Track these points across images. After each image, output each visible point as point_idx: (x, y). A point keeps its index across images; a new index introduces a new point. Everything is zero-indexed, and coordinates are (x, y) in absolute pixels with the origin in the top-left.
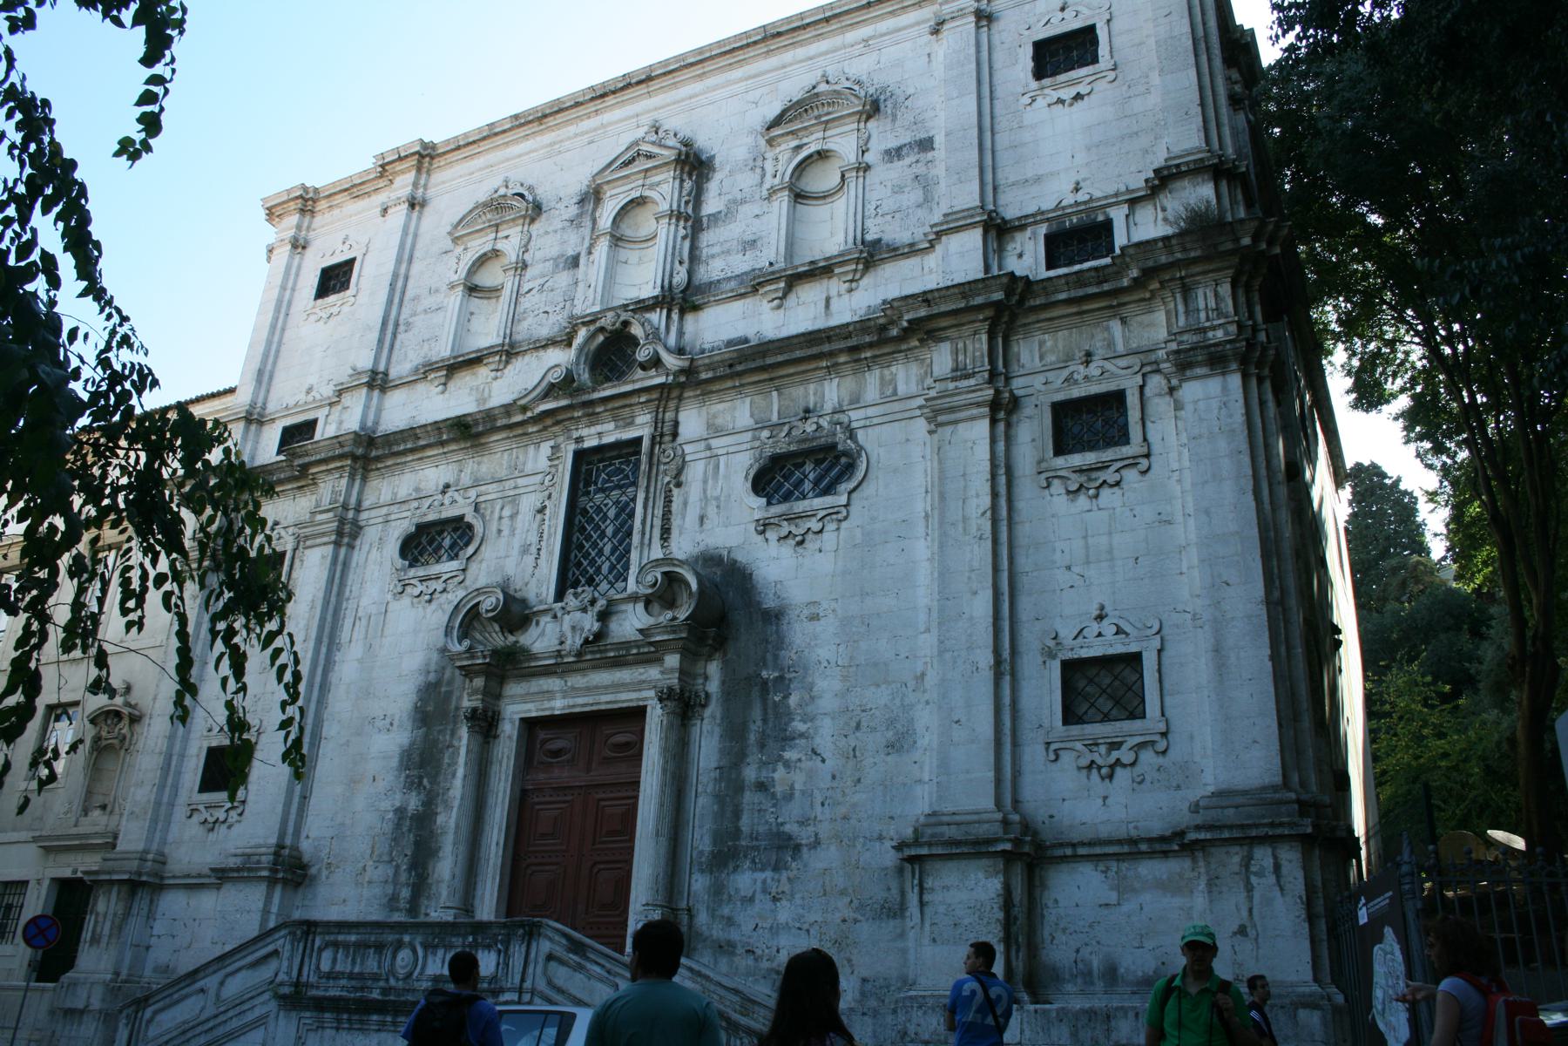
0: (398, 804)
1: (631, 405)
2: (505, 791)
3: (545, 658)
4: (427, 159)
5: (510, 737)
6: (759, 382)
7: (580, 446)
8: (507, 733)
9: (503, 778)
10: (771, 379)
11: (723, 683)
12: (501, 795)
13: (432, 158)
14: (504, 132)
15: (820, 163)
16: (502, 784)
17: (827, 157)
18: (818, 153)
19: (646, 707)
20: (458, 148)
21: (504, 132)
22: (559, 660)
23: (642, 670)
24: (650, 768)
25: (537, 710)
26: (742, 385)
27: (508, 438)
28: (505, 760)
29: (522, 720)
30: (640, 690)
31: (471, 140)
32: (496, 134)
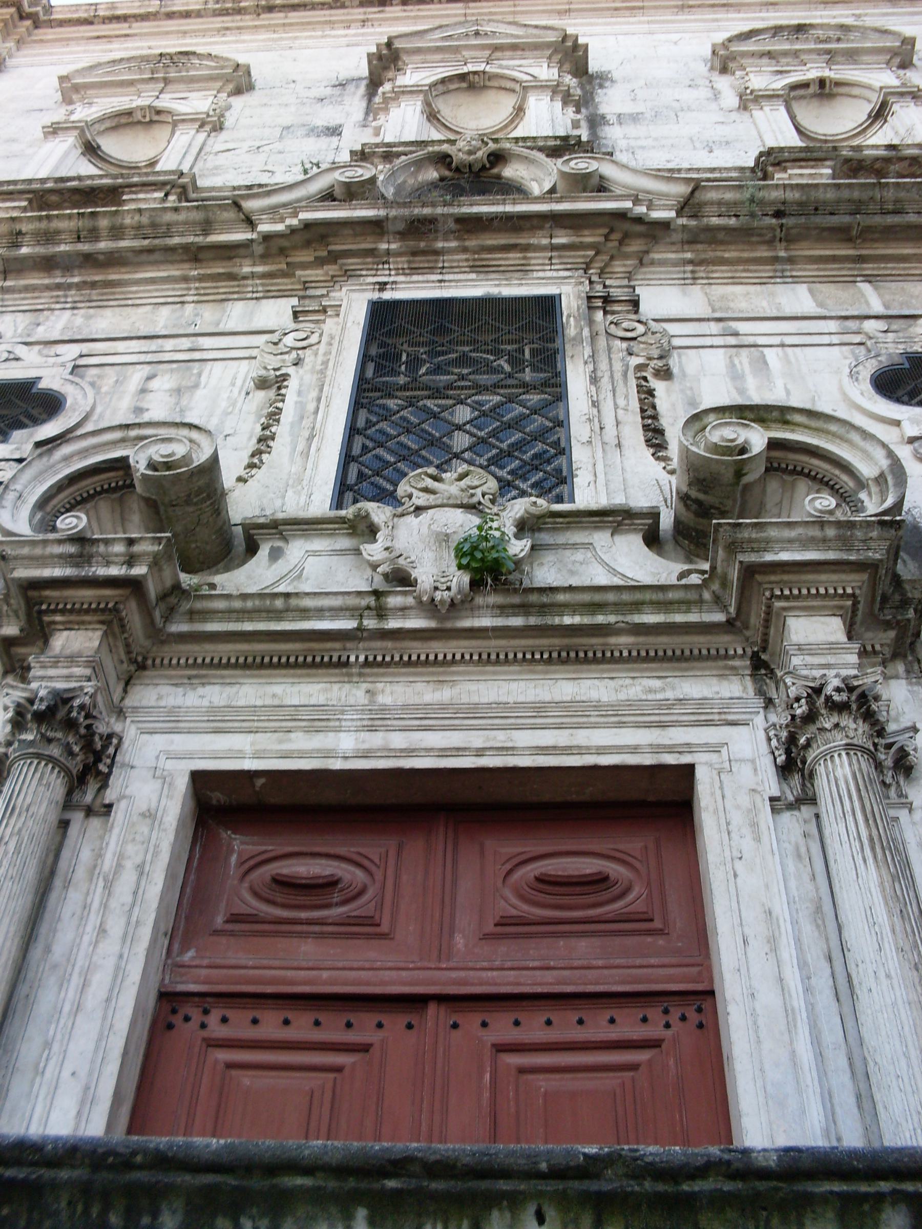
0: (608, 117)
1: (526, 248)
2: (119, 973)
3: (320, 613)
4: (28, 23)
5: (150, 816)
6: (834, 259)
7: (387, 295)
8: (142, 805)
9: (116, 927)
10: (861, 259)
11: (436, 1191)
12: (100, 982)
13: (37, 25)
14: (187, 15)
15: (815, 103)
16: (110, 947)
17: (831, 96)
18: (822, 82)
19: (690, 769)
20: (88, 22)
21: (187, 15)
22: (370, 623)
23: (657, 683)
24: (756, 929)
25: (257, 756)
26: (791, 260)
27: (186, 279)
28: (128, 878)
29: (198, 777)
30: (662, 725)
31: (119, 12)
32: (170, 16)
